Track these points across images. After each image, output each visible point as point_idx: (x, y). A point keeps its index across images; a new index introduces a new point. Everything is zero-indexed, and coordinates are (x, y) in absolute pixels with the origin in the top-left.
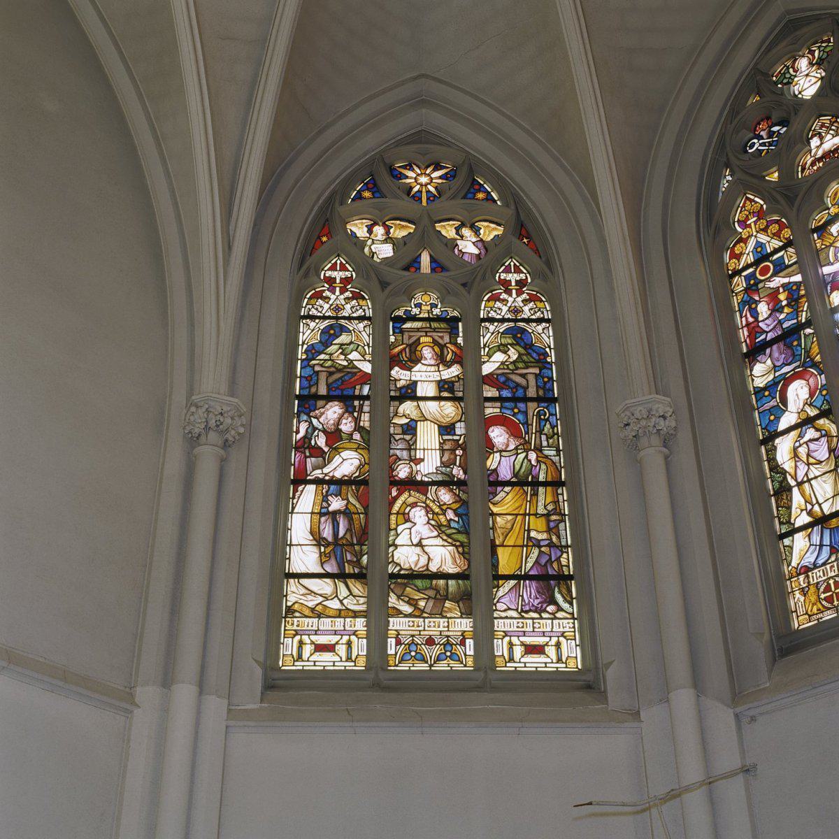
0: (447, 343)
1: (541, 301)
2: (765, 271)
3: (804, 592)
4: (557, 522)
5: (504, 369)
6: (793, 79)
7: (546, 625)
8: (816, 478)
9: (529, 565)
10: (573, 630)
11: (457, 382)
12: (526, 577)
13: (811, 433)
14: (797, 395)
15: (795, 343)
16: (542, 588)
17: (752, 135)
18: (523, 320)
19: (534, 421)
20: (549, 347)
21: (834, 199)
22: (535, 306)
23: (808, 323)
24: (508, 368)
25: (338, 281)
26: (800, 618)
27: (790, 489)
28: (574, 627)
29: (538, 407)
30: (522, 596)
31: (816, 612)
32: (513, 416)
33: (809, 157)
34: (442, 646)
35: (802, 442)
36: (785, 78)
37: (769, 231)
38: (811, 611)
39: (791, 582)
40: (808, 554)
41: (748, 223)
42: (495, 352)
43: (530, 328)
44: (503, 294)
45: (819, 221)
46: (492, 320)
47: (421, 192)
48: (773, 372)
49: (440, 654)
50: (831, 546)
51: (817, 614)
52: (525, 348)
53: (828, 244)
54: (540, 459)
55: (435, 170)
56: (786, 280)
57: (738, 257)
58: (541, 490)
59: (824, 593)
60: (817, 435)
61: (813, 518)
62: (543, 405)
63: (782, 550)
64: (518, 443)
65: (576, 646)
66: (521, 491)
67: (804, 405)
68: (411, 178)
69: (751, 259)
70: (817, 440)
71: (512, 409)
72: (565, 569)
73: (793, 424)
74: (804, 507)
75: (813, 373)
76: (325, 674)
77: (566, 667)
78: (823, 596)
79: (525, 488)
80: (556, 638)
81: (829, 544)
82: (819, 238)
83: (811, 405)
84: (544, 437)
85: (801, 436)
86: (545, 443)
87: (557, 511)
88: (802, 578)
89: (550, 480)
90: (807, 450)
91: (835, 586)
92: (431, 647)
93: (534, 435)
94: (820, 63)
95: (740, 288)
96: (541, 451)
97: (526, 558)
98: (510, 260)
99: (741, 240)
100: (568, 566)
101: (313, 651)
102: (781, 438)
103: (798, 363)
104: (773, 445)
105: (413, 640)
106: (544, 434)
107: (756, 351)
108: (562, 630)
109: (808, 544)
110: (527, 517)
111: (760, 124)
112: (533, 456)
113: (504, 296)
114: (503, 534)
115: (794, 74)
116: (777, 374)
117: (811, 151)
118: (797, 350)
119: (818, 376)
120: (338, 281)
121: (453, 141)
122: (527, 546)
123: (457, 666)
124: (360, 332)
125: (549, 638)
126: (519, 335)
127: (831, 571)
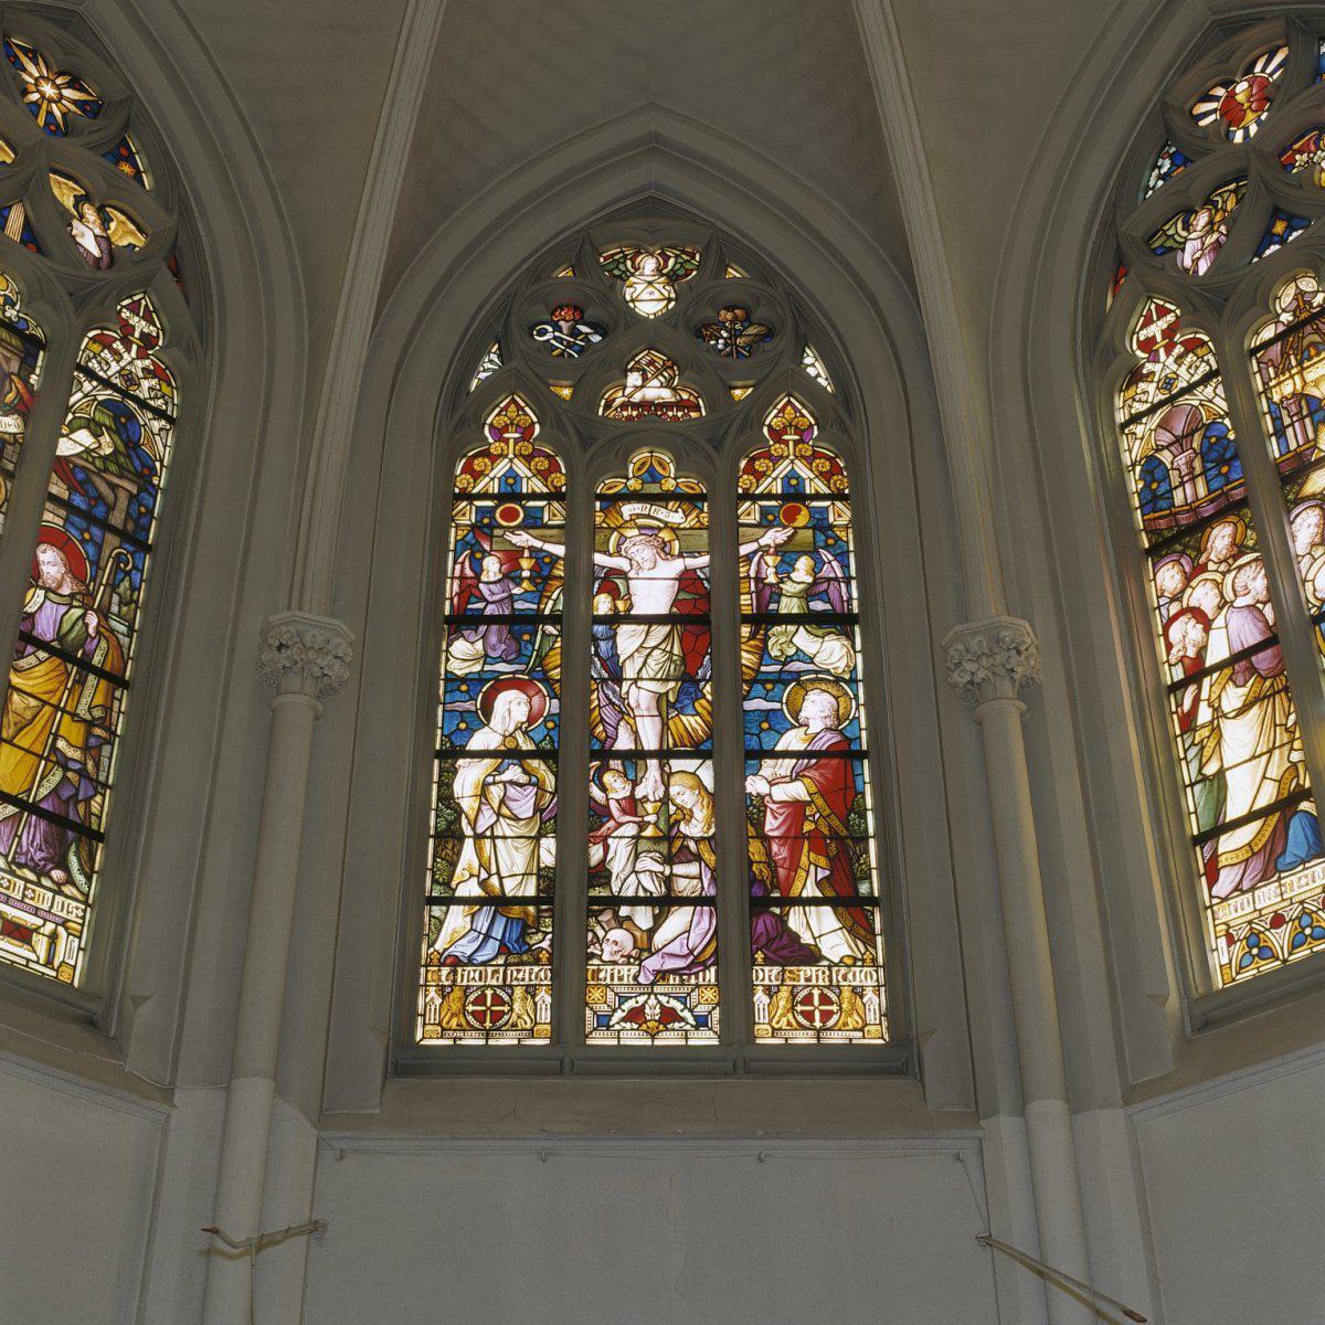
0: (12, 373)
1: (169, 384)
2: (510, 515)
3: (441, 990)
4: (101, 741)
5: (87, 460)
6: (628, 277)
7: (44, 898)
8: (504, 837)
9: (44, 792)
10: (81, 921)
11: (10, 444)
12: (34, 809)
13: (513, 773)
14: (509, 710)
15: (526, 637)
16: (52, 837)
17: (547, 317)
18: (136, 399)
19: (109, 565)
20: (162, 461)
21: (639, 469)
22: (158, 387)
23: (554, 619)
24: (93, 463)
25: (1159, 338)
26: (428, 1028)
27: (461, 838)
28: (83, 918)
29: (120, 547)
30: (20, 837)
31: (454, 1027)
32: (79, 541)
33: (620, 394)
34: (1296, 922)
35: (498, 778)
36: (617, 267)
37: (533, 464)
38: (448, 1023)
39: (427, 971)
40: (464, 941)
41: (506, 435)
42: (81, 428)
43: (144, 417)
44: (118, 343)
45: (611, 488)
46: (91, 375)
47: (40, 107)
48: (482, 662)
50: (502, 941)
51: (455, 1030)
52: (126, 445)
53: (612, 525)
54: (102, 630)
55: (70, 85)
56: (538, 544)
57: (477, 476)
58: (92, 679)
59: (474, 1003)
60: (523, 779)
61: (487, 893)
62: (127, 546)
63: (427, 919)
64: (76, 589)
65: (80, 949)
66: (62, 667)
67: (516, 730)
68: (30, 75)
69: (494, 488)
70: (521, 785)
71: (82, 532)
72: (94, 819)
73: (491, 748)
74: (475, 872)
75: (541, 691)
78: (470, 1008)
79: (70, 666)
80: (53, 926)
81: (499, 938)
82: (601, 510)
83: (525, 733)
84: (115, 598)
85: (499, 770)
86: (115, 609)
87: (106, 723)
88: (445, 971)
89: (107, 669)
90: (502, 794)
91: (481, 1005)
93: (102, 588)
94: (672, 278)
95: (464, 521)
96: (106, 618)
97: (40, 781)
98: (142, 295)
99: (486, 454)
100: (100, 818)
102: (468, 760)
103: (523, 667)
104: (453, 765)
105: (1251, 928)
106: (117, 593)
107: (463, 621)
108: (64, 914)
109: (469, 927)
110: (59, 713)
111: (562, 310)
112: (93, 620)
113: (118, 345)
114: (15, 724)
115: (632, 271)
116: (487, 668)
117: (625, 387)
118: (526, 648)
119: (547, 699)
120: (1159, 338)
121: (117, 59)
122: (48, 760)
124: (1211, 401)
126: (123, 420)
127: (492, 978)
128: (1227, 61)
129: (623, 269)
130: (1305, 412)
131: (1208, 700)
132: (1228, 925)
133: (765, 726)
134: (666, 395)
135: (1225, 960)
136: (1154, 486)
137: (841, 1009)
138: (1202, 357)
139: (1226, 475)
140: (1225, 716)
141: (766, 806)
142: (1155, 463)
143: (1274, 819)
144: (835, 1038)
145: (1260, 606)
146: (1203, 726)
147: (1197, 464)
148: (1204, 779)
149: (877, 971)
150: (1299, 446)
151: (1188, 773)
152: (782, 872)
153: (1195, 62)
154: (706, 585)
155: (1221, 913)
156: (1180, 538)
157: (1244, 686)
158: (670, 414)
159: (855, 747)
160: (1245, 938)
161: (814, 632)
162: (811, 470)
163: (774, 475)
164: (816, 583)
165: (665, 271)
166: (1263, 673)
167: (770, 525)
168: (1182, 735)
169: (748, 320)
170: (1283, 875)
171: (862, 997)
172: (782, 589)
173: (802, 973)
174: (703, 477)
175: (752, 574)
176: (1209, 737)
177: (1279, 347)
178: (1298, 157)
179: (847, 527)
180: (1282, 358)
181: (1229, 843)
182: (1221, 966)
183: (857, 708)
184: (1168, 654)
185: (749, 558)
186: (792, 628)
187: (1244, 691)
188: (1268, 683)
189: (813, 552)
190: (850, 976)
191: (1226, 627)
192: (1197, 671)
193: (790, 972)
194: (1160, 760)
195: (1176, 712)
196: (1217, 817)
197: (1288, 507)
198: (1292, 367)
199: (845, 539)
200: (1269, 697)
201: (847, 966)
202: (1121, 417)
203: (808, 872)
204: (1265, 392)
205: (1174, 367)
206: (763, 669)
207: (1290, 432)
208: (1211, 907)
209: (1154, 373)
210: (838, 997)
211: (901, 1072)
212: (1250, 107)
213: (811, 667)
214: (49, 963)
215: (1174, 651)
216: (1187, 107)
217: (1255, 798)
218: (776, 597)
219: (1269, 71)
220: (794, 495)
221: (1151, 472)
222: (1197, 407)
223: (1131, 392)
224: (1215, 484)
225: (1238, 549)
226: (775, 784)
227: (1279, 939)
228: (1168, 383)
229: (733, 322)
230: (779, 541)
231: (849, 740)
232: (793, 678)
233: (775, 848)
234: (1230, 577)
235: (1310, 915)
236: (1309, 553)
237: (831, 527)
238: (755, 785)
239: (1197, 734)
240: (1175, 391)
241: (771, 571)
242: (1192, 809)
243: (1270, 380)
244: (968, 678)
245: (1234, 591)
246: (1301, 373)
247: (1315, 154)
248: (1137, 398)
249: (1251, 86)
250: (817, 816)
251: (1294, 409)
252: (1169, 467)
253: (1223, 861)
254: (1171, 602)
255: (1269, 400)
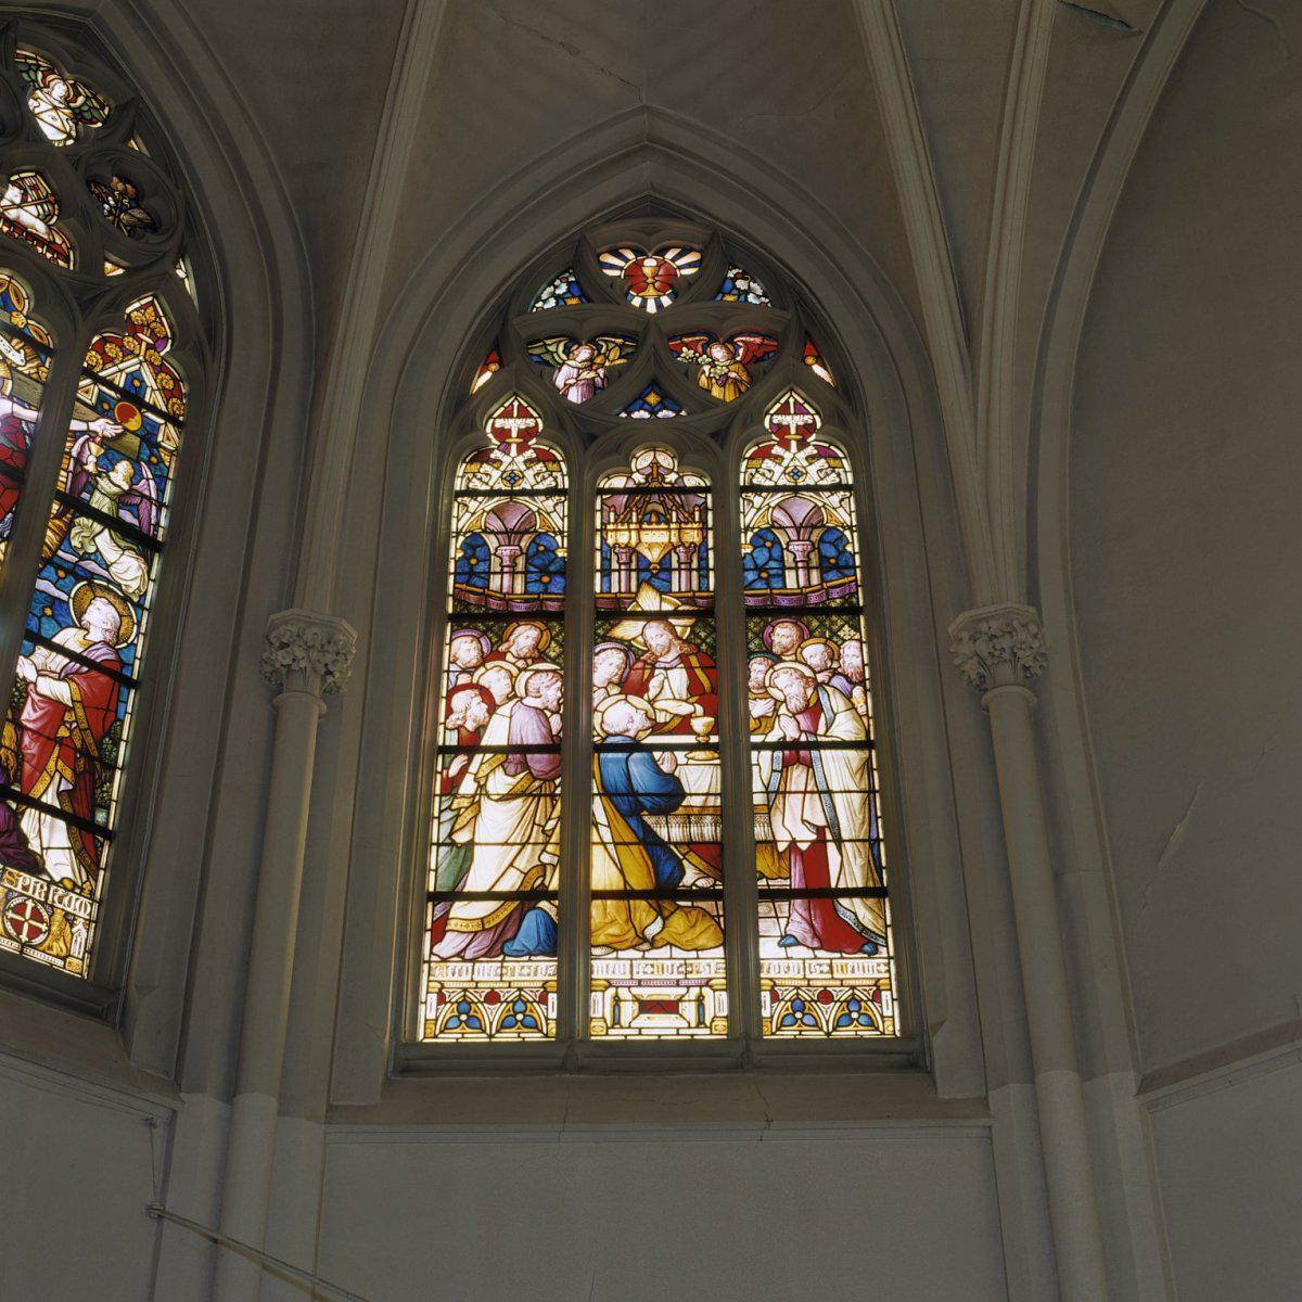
10: (887, 975)
25: (514, 434)
28: (889, 971)
34: (511, 1005)
49: (450, 1018)
65: (893, 1000)
76: (660, 1047)
77: (711, 1034)
92: (826, 1006)
94: (77, 116)
101: (636, 1014)
105: (465, 996)
115: (42, 85)
120: (514, 434)
123: (533, 1037)
124: (548, 514)
125: (685, 990)
128: (649, 234)
129: (33, 77)
130: (633, 566)
131: (476, 775)
132: (442, 985)
133: (48, 612)
134: (40, 228)
135: (431, 1016)
136: (473, 561)
137: (49, 930)
138: (552, 472)
139: (546, 584)
140: (488, 795)
141: (28, 694)
142: (480, 542)
143: (512, 906)
144: (38, 957)
145: (548, 714)
146: (463, 796)
147: (521, 562)
148: (453, 844)
149: (92, 905)
150: (620, 592)
151: (438, 832)
152: (27, 767)
153: (619, 219)
154: (28, 441)
155: (437, 972)
156: (490, 620)
157: (513, 776)
158: (40, 250)
159: (126, 672)
160: (456, 1002)
161: (117, 540)
162: (155, 380)
163: (121, 366)
164: (130, 493)
165: (72, 105)
166: (534, 773)
167: (103, 414)
168: (441, 796)
169: (137, 201)
170: (507, 958)
171: (72, 926)
172: (97, 483)
173: (21, 879)
174: (54, 330)
175: (74, 453)
176: (467, 808)
177: (625, 500)
178: (684, 349)
179: (171, 452)
180: (626, 508)
181: (460, 910)
182: (426, 1020)
183: (137, 635)
184: (447, 718)
185: (76, 435)
186: (97, 527)
187: (513, 781)
188: (537, 783)
189: (135, 462)
190: (66, 900)
191: (511, 717)
192: (470, 745)
193: (11, 874)
194: (420, 810)
195: (441, 773)
196: (457, 883)
197: (596, 640)
198: (632, 523)
199: (167, 464)
200: (534, 796)
201: (65, 888)
202: (459, 485)
203: (52, 778)
204: (601, 530)
205: (523, 467)
206: (60, 553)
207: (615, 576)
208: (429, 962)
209: (501, 462)
210: (50, 917)
211: (99, 1015)
212: (653, 284)
213: (105, 573)
214: (700, 1023)
215: (453, 717)
216: (598, 251)
217: (498, 880)
218: (90, 488)
219: (680, 262)
220: (132, 395)
221: (474, 548)
222: (533, 513)
223: (474, 467)
224: (534, 588)
225: (539, 655)
226: (43, 675)
227: (492, 1014)
228: (512, 478)
229: (124, 193)
230: (107, 434)
231: (124, 664)
232: (88, 577)
233: (27, 740)
234: (525, 676)
235: (525, 1003)
236: (606, 688)
237: (158, 446)
238: (25, 669)
239: (456, 801)
240: (517, 488)
241: (92, 459)
242: (433, 866)
243: (609, 523)
244: (288, 661)
245: (526, 690)
246: (639, 530)
247: (701, 356)
248: (479, 476)
249: (659, 266)
250: (75, 725)
251: (624, 558)
252: (492, 551)
253: (452, 925)
254: (461, 672)
255: (603, 540)
